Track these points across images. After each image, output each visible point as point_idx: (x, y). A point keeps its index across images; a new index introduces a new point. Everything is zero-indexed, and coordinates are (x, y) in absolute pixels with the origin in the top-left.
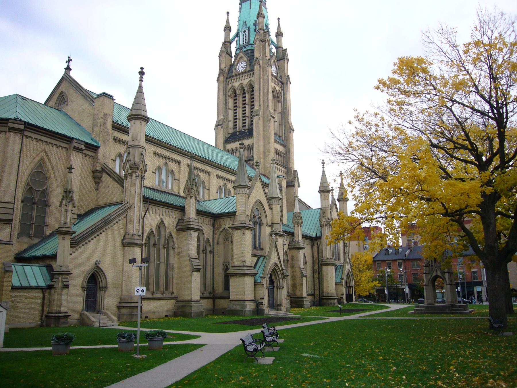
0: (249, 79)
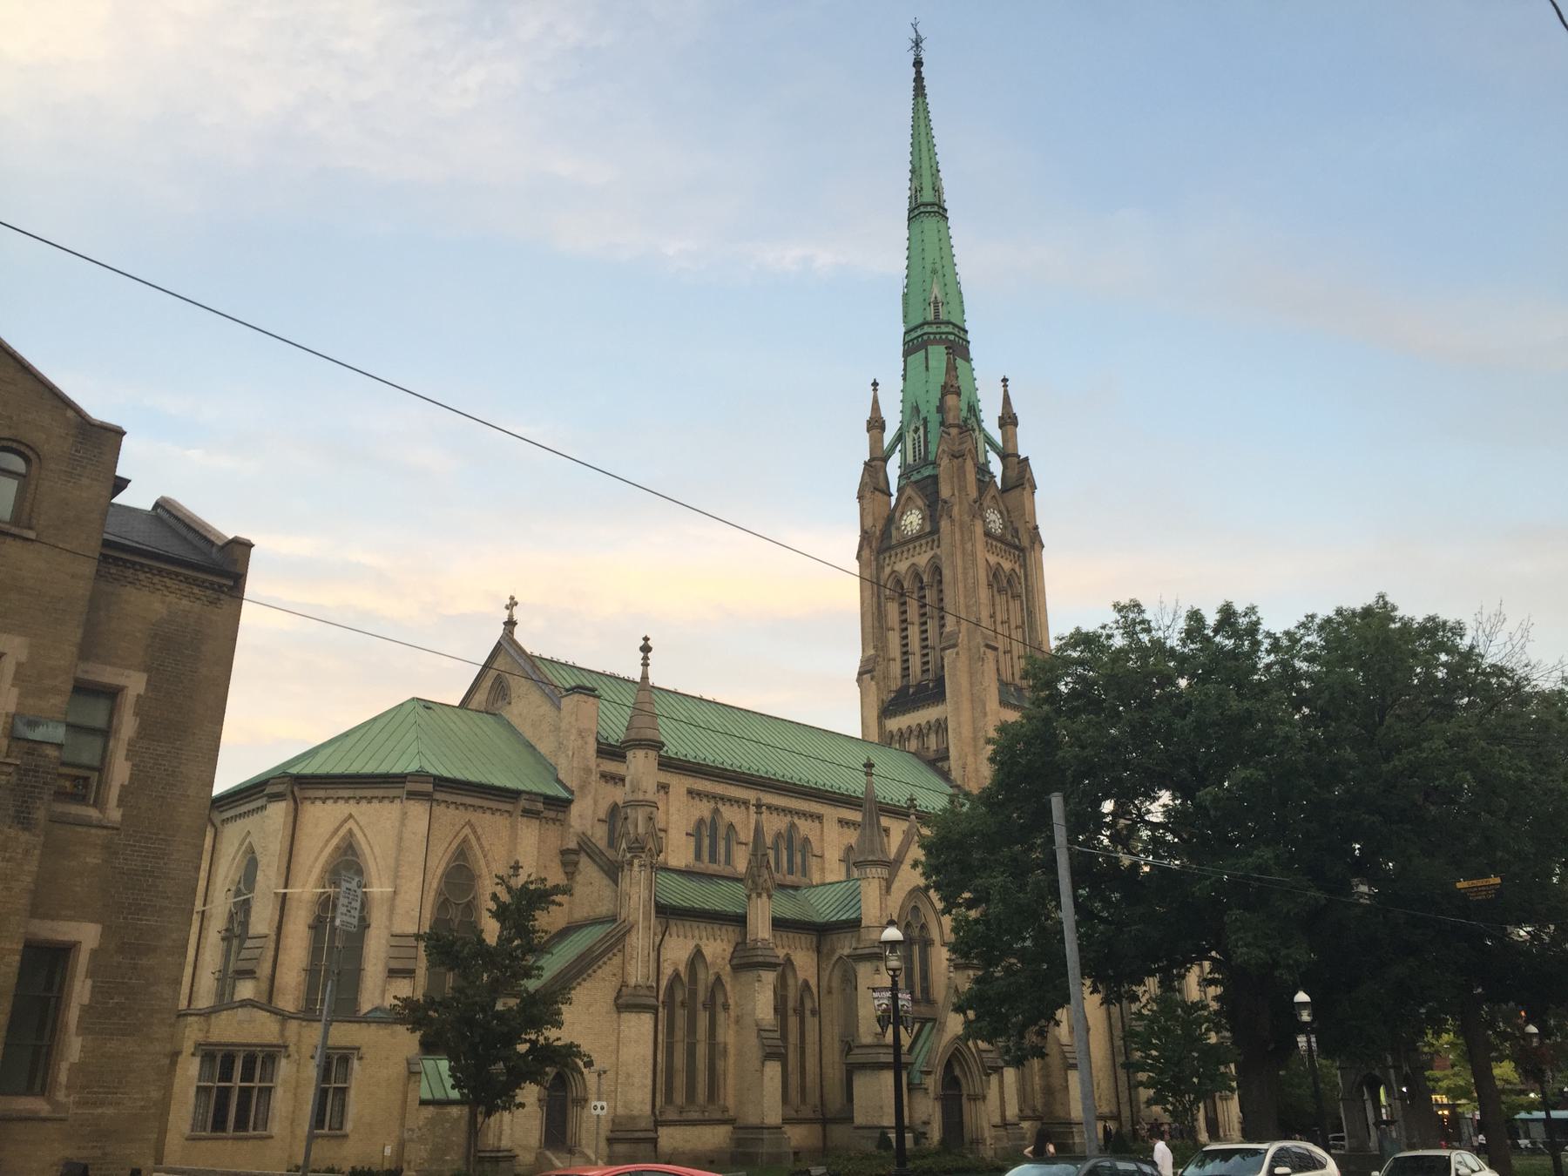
0: (930, 554)
